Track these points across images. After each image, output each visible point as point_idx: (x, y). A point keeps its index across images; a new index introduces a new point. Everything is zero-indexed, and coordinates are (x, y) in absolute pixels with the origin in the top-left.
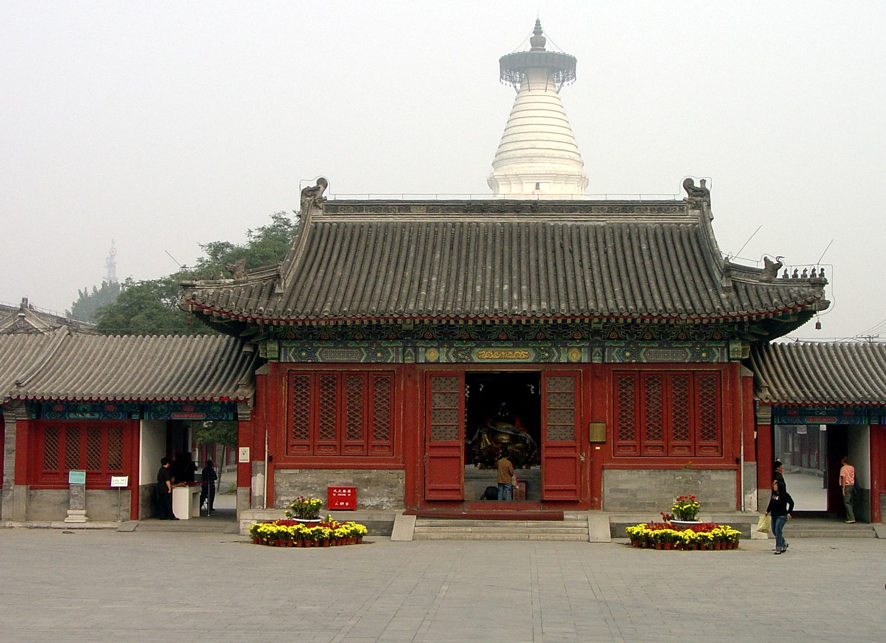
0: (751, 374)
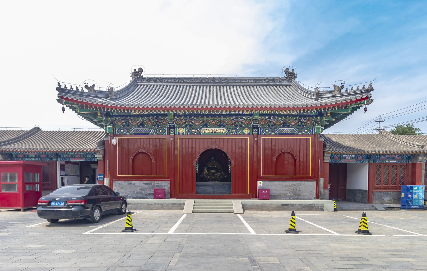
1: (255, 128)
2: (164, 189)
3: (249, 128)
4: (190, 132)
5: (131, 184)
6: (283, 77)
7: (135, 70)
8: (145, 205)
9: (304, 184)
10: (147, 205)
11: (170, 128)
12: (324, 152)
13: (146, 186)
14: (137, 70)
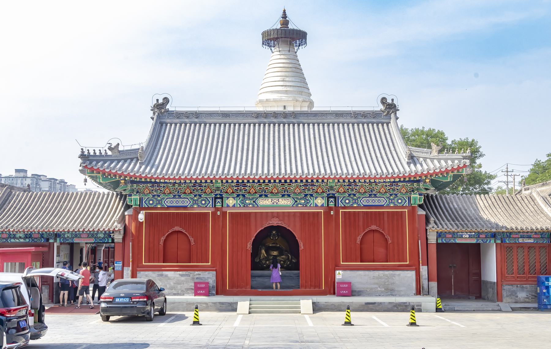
0: (424, 213)
1: (331, 197)
2: (208, 283)
3: (323, 198)
4: (243, 203)
5: (162, 275)
6: (379, 109)
7: (158, 100)
8: (185, 305)
9: (399, 275)
10: (187, 304)
11: (216, 198)
12: (426, 230)
13: (183, 278)
14: (161, 101)
